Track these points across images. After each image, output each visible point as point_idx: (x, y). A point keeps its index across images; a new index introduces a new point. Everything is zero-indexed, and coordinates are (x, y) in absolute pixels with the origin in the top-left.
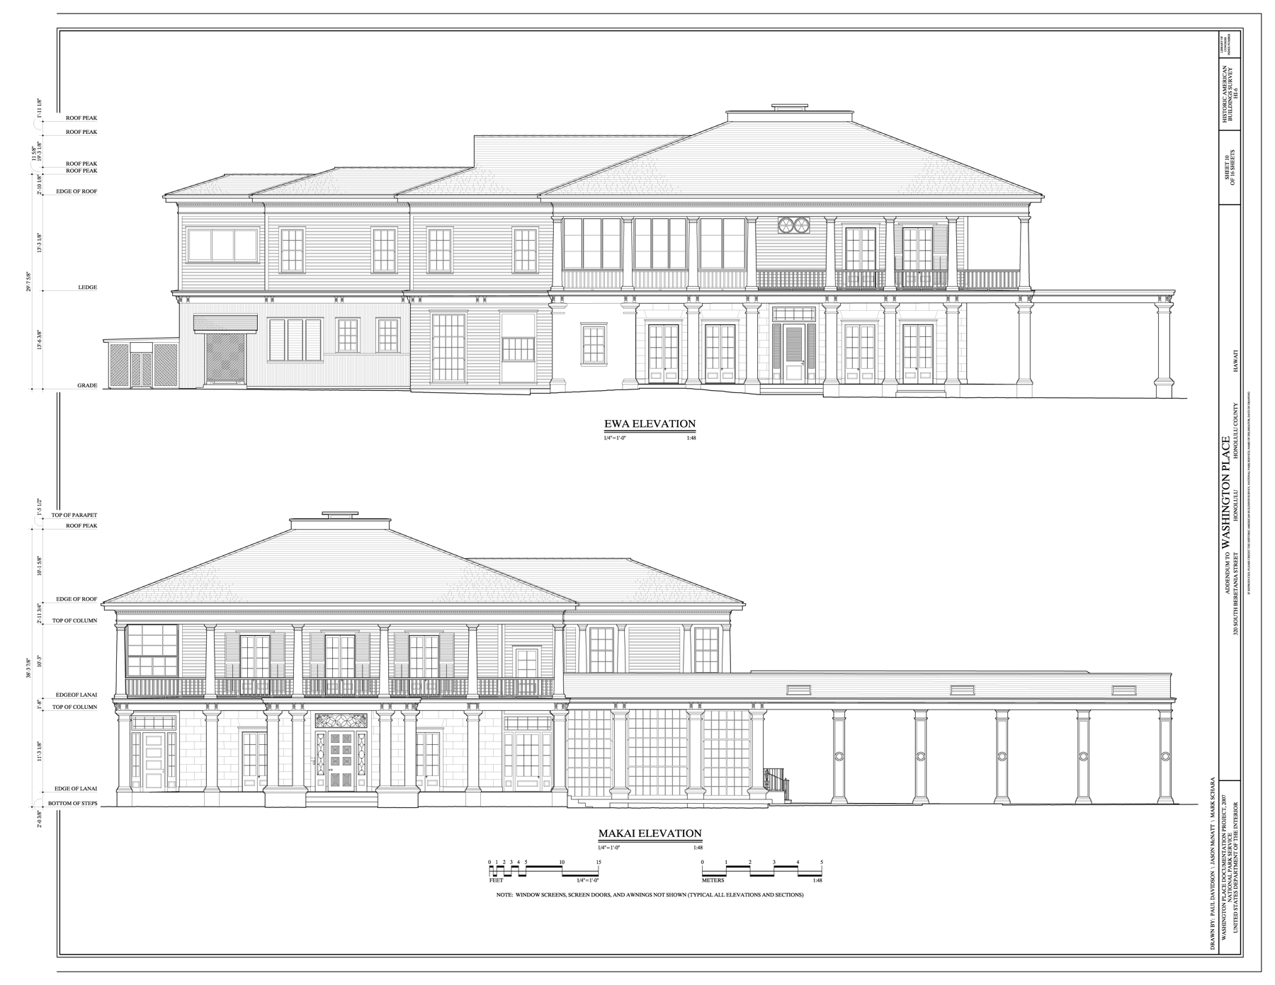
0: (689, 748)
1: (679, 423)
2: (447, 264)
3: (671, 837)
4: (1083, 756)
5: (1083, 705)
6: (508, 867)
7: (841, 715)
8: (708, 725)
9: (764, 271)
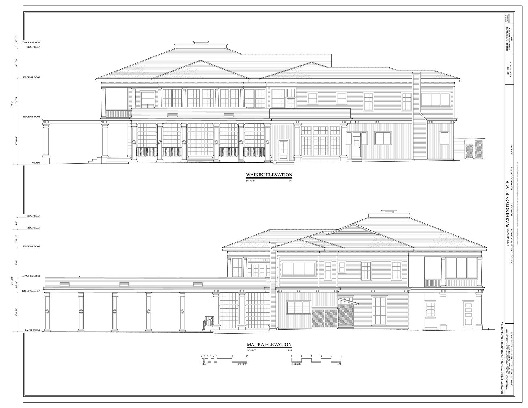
0: (239, 309)
1: (285, 175)
2: (371, 107)
3: (279, 346)
4: (81, 311)
5: (115, 292)
6: (209, 358)
7: (183, 295)
8: (247, 299)
9: (109, 110)
